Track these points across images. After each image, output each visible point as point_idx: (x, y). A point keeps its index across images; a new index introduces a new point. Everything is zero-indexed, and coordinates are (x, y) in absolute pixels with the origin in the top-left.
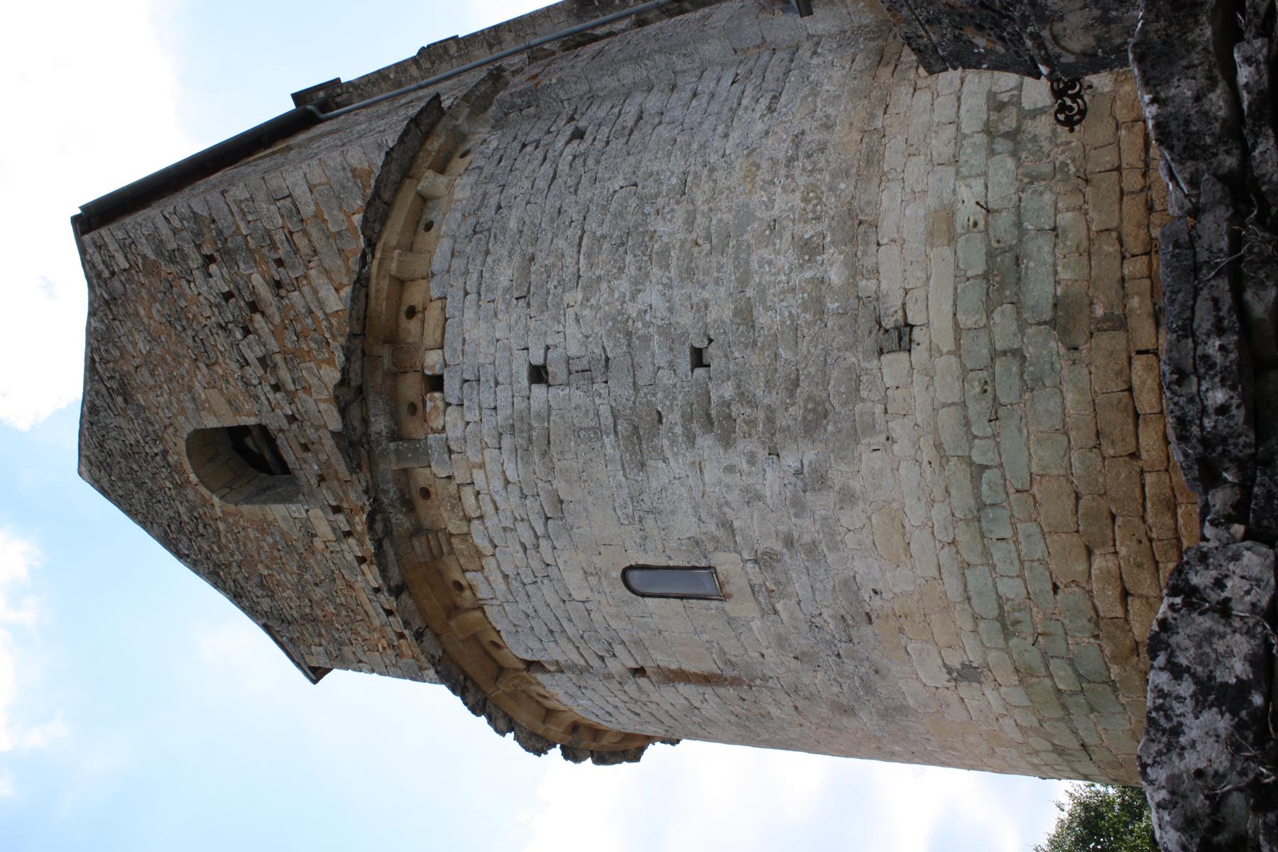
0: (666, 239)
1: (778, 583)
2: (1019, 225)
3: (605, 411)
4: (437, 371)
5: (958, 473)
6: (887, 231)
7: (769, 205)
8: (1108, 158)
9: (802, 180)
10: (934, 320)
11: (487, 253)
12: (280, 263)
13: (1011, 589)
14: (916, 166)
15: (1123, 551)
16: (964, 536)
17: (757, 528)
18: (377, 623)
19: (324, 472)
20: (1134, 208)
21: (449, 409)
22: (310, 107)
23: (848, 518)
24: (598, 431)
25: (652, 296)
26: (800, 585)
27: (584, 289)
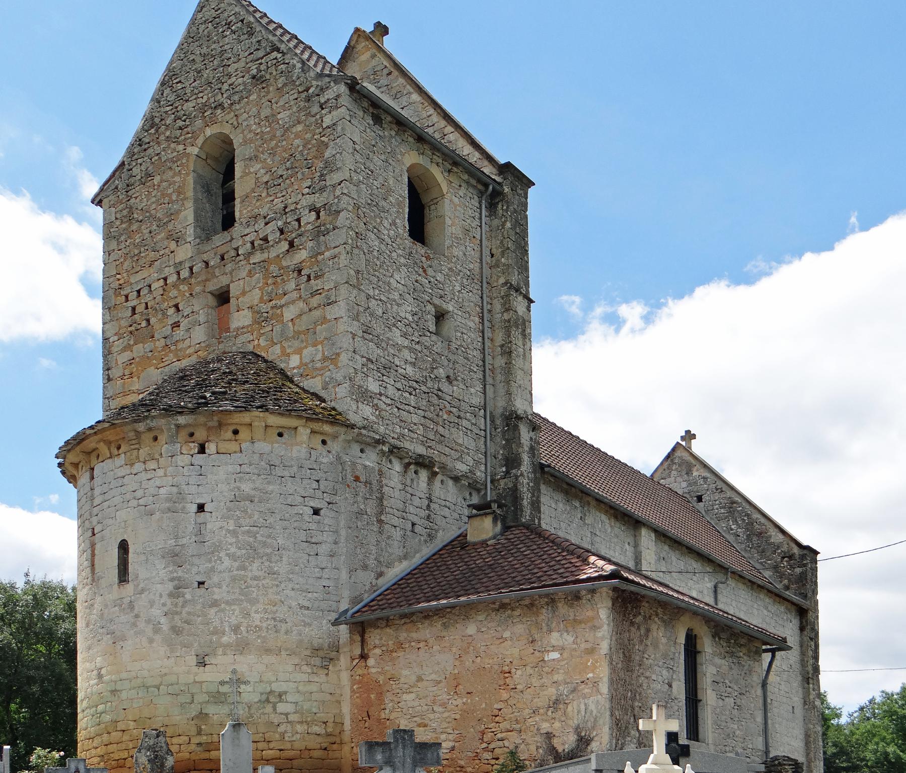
0: (250, 568)
3: (184, 541)
4: (207, 451)
5: (156, 682)
7: (257, 612)
9: (264, 625)
11: (259, 475)
13: (124, 695)
16: (139, 681)
17: (142, 602)
23: (144, 639)
24: (176, 537)
25: (227, 562)
27: (234, 530)
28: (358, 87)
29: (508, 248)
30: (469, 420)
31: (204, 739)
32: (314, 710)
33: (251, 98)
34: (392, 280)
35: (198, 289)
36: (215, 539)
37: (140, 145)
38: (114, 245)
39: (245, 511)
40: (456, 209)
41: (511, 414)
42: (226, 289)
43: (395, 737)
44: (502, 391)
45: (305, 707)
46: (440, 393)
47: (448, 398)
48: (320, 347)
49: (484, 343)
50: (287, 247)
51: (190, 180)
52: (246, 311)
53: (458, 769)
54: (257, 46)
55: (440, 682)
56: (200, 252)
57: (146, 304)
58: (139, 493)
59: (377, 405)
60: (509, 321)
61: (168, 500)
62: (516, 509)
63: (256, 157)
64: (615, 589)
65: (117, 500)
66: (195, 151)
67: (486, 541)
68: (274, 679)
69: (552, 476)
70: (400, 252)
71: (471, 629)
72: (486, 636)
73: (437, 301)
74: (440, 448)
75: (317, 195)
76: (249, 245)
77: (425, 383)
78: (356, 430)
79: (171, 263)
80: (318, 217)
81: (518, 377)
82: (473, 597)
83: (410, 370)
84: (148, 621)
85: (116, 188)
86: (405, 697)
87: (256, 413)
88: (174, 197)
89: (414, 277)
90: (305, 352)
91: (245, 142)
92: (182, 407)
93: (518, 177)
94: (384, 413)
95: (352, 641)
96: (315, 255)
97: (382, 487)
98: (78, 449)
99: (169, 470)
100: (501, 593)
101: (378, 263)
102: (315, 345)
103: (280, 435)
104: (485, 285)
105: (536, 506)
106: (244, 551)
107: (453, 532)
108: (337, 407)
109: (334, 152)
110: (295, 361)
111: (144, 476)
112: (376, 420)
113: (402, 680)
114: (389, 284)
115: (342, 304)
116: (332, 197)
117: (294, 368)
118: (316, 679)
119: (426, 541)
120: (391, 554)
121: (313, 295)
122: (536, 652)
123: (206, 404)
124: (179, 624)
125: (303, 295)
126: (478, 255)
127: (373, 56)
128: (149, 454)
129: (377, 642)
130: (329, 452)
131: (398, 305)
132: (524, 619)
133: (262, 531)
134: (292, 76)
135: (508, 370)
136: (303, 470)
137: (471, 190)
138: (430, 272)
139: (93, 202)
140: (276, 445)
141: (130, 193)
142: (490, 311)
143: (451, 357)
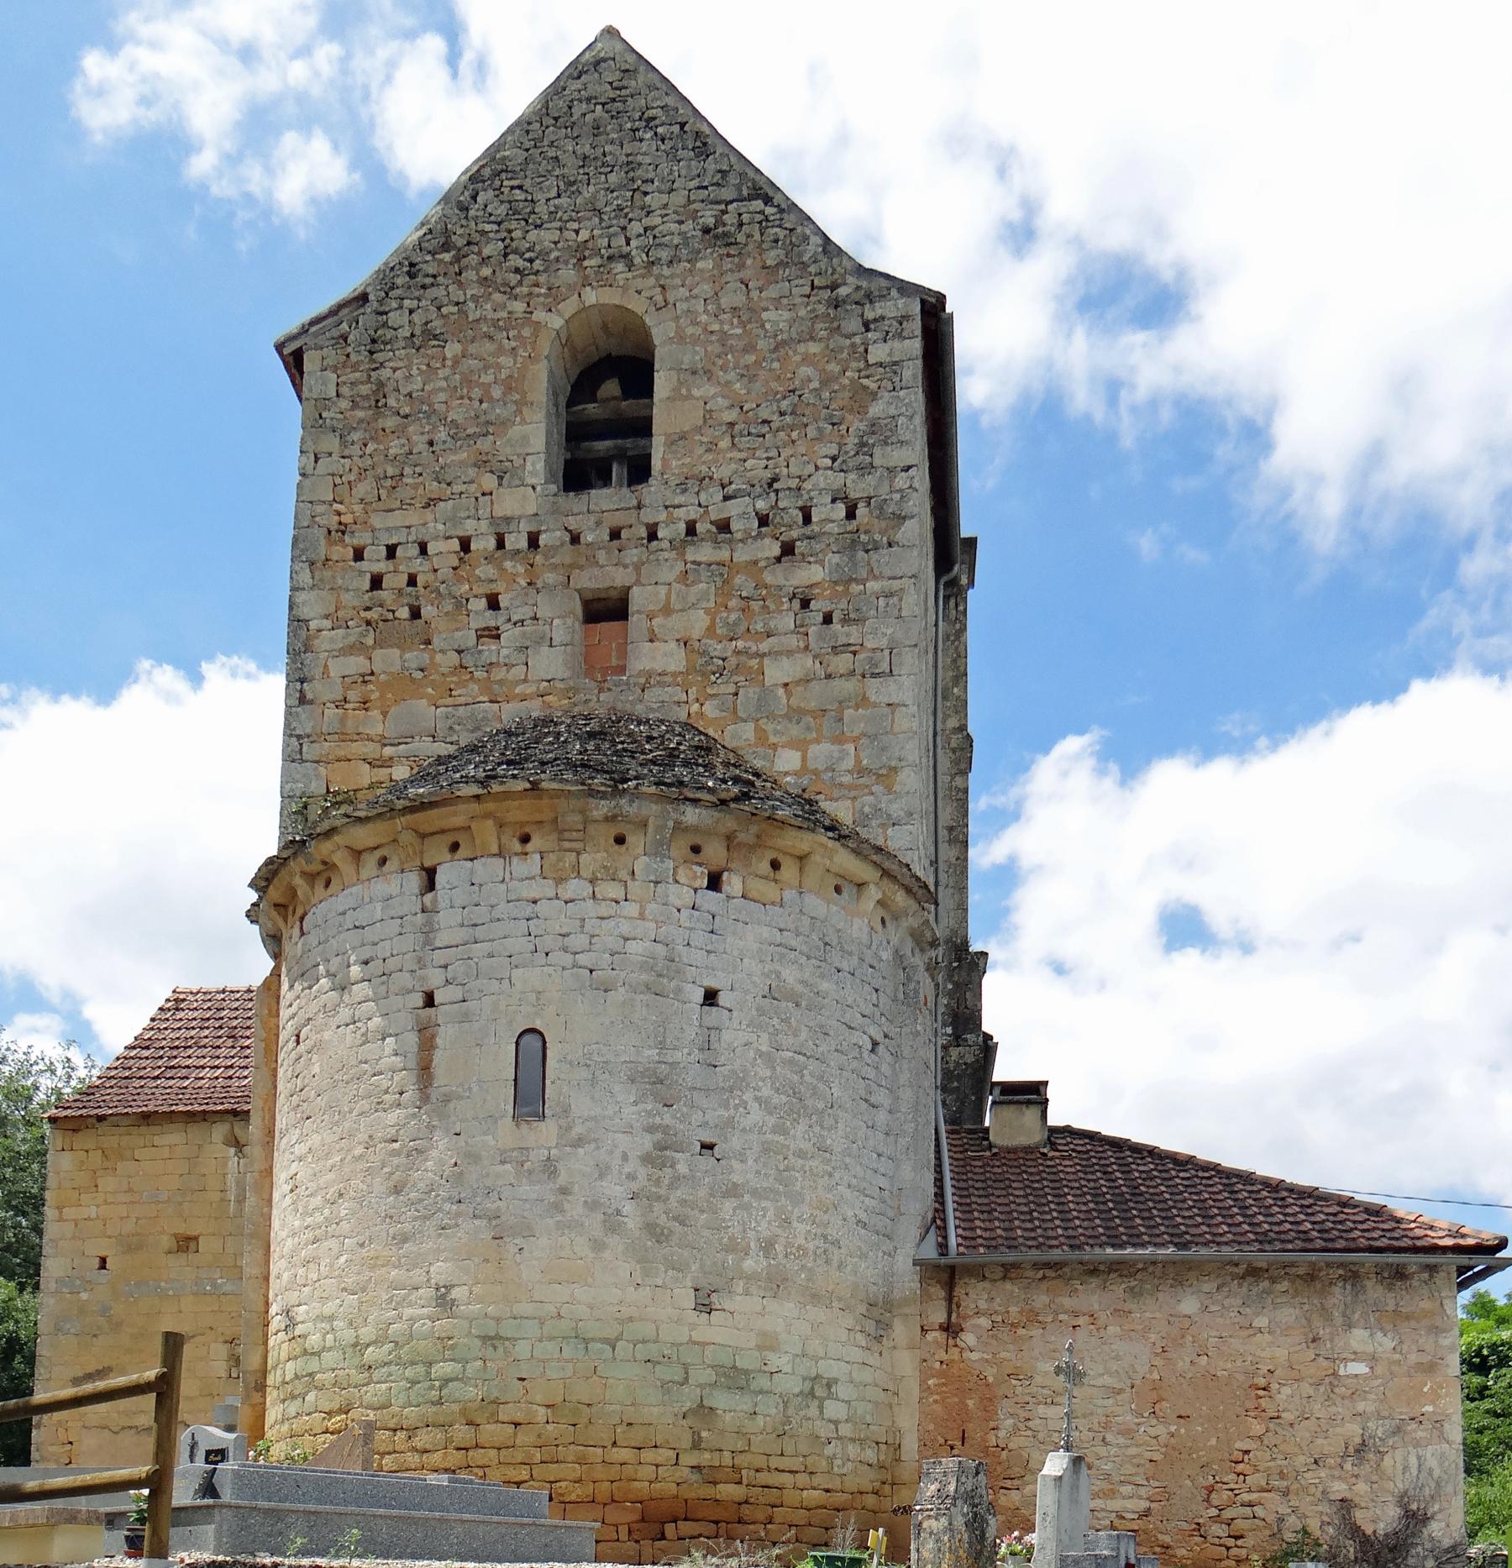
1: (530, 1172)
2: (761, 1392)
3: (678, 1056)
4: (725, 887)
5: (611, 1332)
7: (800, 1219)
8: (789, 1450)
9: (811, 1246)
10: (715, 1330)
11: (809, 958)
12: (828, 619)
13: (522, 1349)
15: (550, 1427)
16: (565, 1325)
18: (377, 521)
19: (582, 548)
20: (761, 1462)
22: (956, 568)
23: (582, 1247)
24: (662, 1046)
25: (756, 1115)
26: (526, 1190)
27: (769, 1053)
31: (706, 1458)
33: (699, 265)
50: (777, 551)
52: (673, 645)
55: (1120, 1391)
61: (643, 967)
66: (556, 322)
71: (1189, 1305)
76: (682, 526)
90: (814, 750)
91: (680, 338)
102: (839, 740)
113: (1038, 1380)
125: (812, 645)
129: (983, 1305)
134: (800, 255)
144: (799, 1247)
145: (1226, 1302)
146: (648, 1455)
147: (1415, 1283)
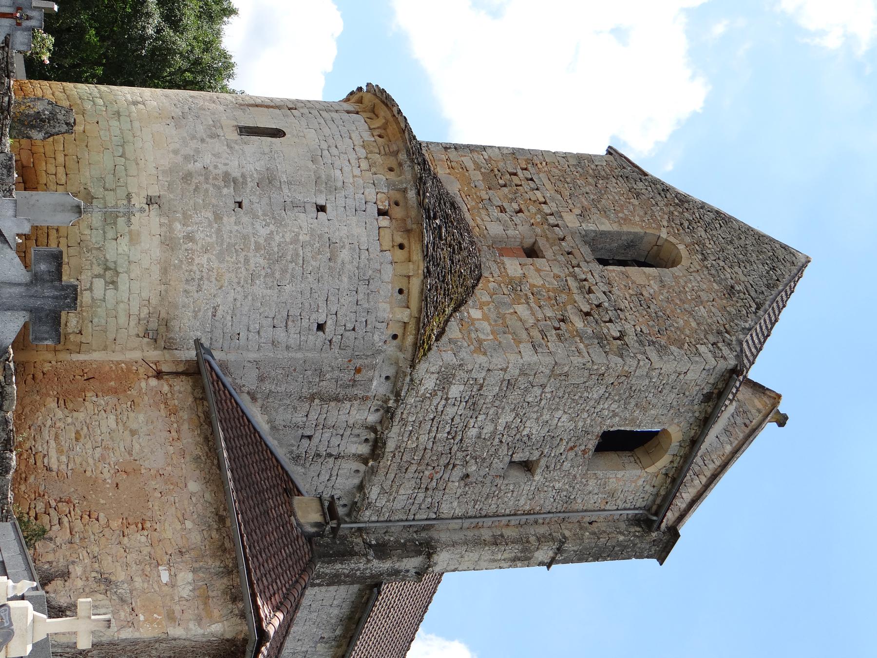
3: (286, 191)
4: (381, 217)
6: (156, 240)
7: (209, 260)
8: (71, 250)
9: (195, 268)
13: (114, 123)
14: (145, 263)
16: (130, 138)
17: (218, 146)
21: (374, 201)
23: (178, 146)
24: (289, 183)
25: (264, 232)
27: (298, 240)
28: (735, 376)
29: (599, 538)
30: (424, 500)
32: (95, 320)
34: (561, 412)
35: (538, 230)
36: (288, 221)
37: (663, 190)
38: (573, 162)
39: (319, 252)
40: (631, 482)
41: (433, 547)
42: (540, 255)
43: (68, 287)
44: (456, 537)
45: (99, 310)
46: (451, 467)
47: (446, 476)
48: (491, 337)
49: (503, 516)
51: (637, 230)
52: (521, 272)
53: (24, 475)
54: (759, 291)
55: (130, 454)
56: (573, 234)
57: (521, 185)
58: (334, 151)
59: (436, 395)
60: (528, 542)
62: (331, 556)
63: (664, 286)
64: (245, 641)
65: (327, 131)
66: (664, 235)
67: (295, 516)
68: (133, 276)
69: (368, 599)
70: (589, 421)
71: (194, 486)
72: (186, 502)
73: (543, 462)
74: (394, 467)
75: (635, 338)
76: (584, 277)
77: (460, 449)
78: (409, 370)
79: (561, 209)
80: (615, 339)
81: (471, 554)
82: (231, 484)
83: (473, 432)
84: (197, 151)
85: (624, 168)
86: (112, 418)
87: (422, 266)
88: (620, 215)
89: (566, 437)
90: (485, 324)
91: (676, 278)
92: (424, 194)
93: (666, 547)
94: (428, 403)
95: (177, 362)
96: (580, 335)
97: (350, 400)
98: (377, 101)
99: (360, 181)
100: (238, 514)
101: (576, 397)
103: (401, 291)
104: (562, 515)
105: (335, 580)
106: (276, 249)
107: (302, 484)
108: (432, 352)
109: (675, 354)
110: (476, 314)
111: (353, 156)
112: (421, 393)
113: (132, 415)
114: (558, 409)
115: (535, 358)
116: (635, 351)
117: (468, 313)
118: (132, 323)
119: (291, 452)
120: (276, 411)
121: (541, 331)
122: (168, 557)
123: (428, 217)
124: (195, 181)
126: (590, 507)
127: (759, 411)
128: (375, 163)
129: (177, 388)
130: (385, 342)
131: (538, 419)
132: (207, 542)
133: (299, 270)
135: (478, 543)
136: (365, 314)
137: (651, 498)
138: (571, 454)
139: (609, 147)
140: (390, 287)
141: (620, 178)
142: (536, 522)
143: (489, 478)
144: (193, 259)
145: (199, 505)
146: (61, 170)
147: (230, 606)
